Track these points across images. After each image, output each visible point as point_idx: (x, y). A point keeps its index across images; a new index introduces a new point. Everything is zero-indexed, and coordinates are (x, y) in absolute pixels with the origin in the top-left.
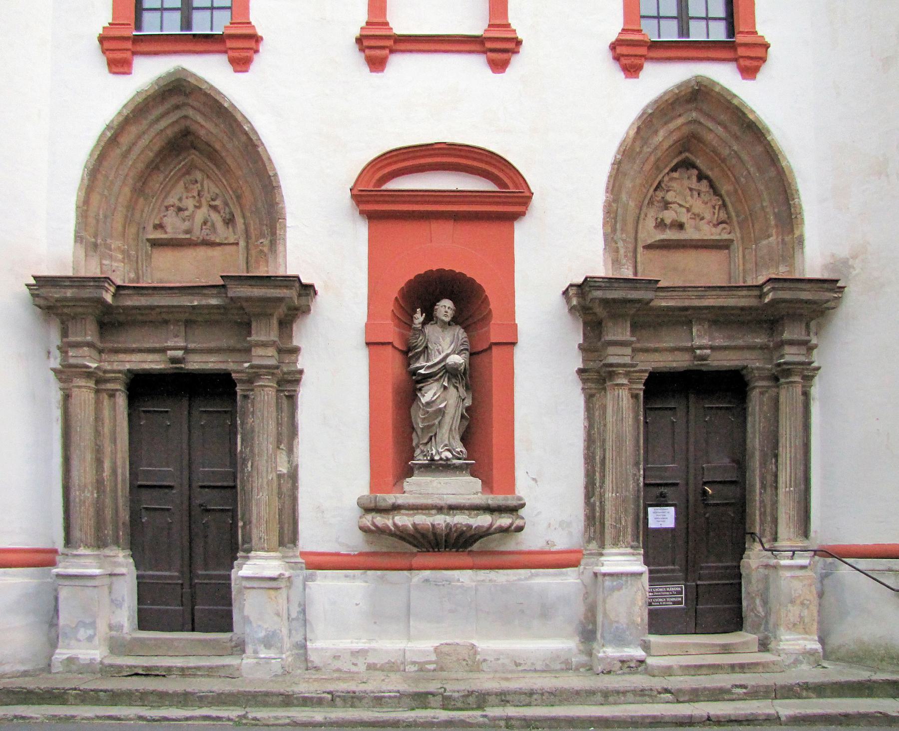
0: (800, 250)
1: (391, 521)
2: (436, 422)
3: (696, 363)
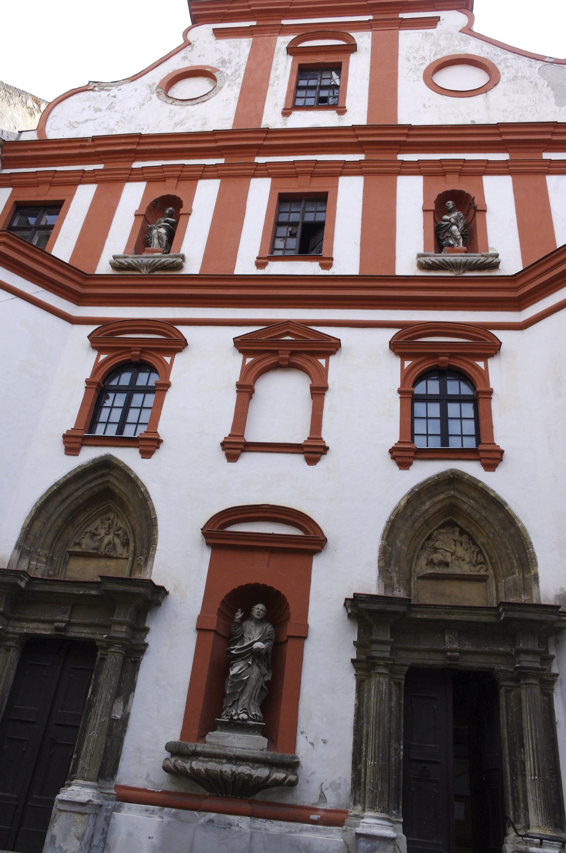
0: (536, 585)
1: (189, 765)
3: (448, 662)
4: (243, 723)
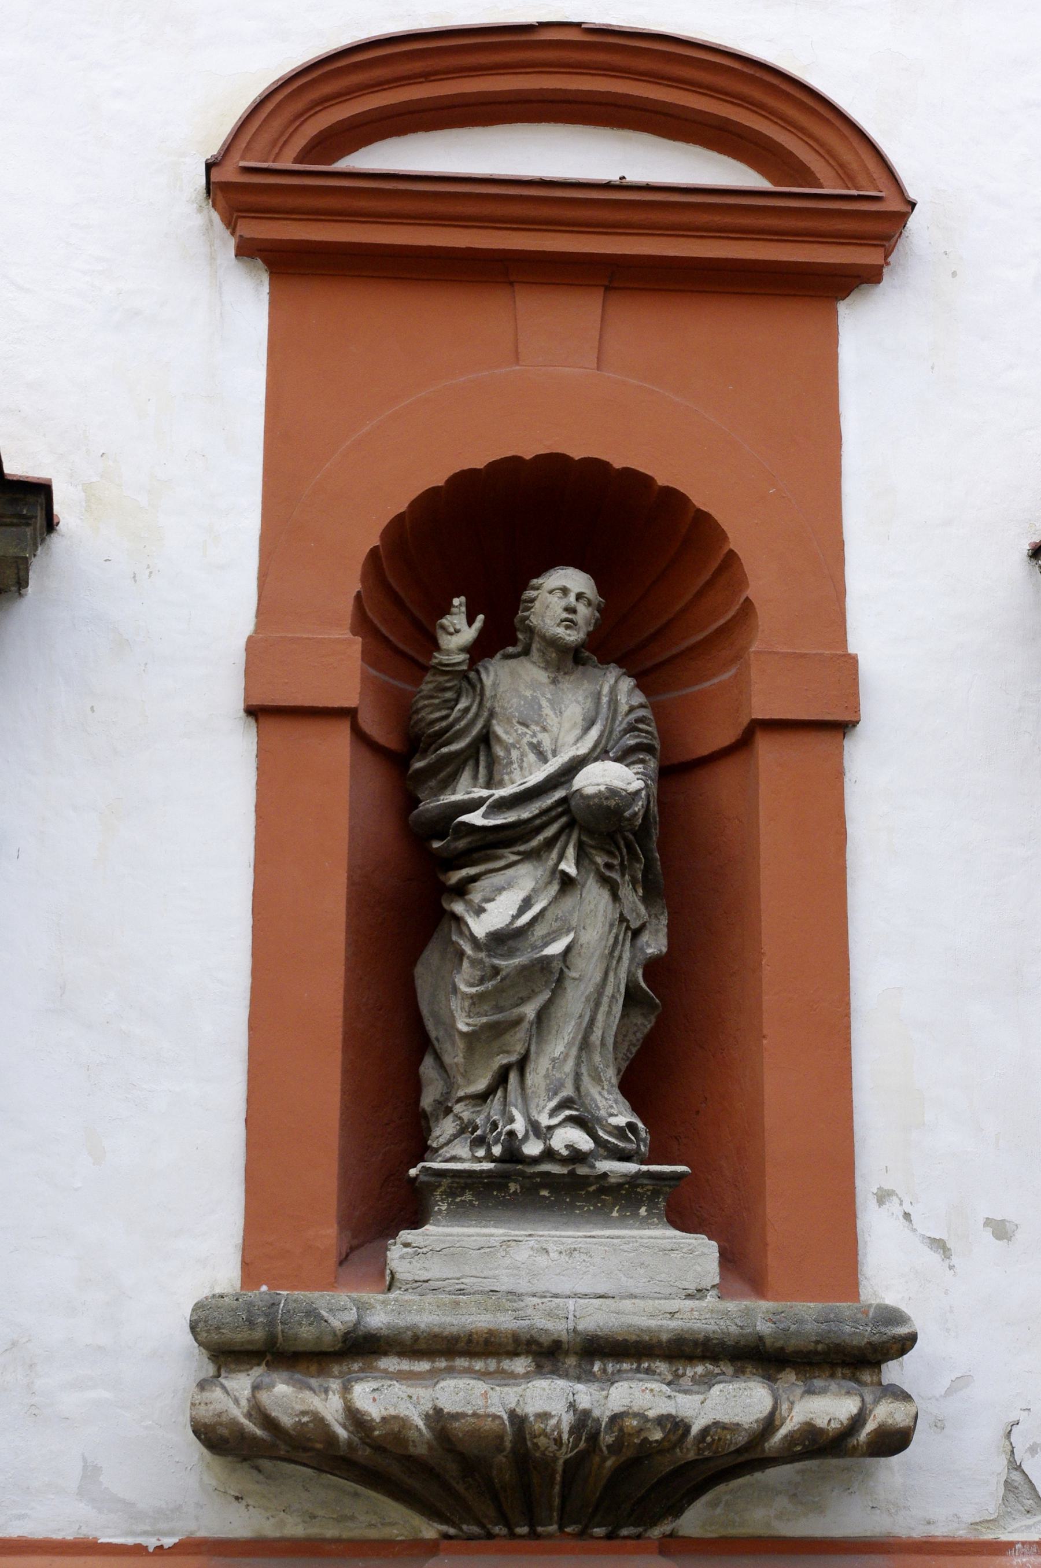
2: (530, 1010)
4: (572, 1173)
